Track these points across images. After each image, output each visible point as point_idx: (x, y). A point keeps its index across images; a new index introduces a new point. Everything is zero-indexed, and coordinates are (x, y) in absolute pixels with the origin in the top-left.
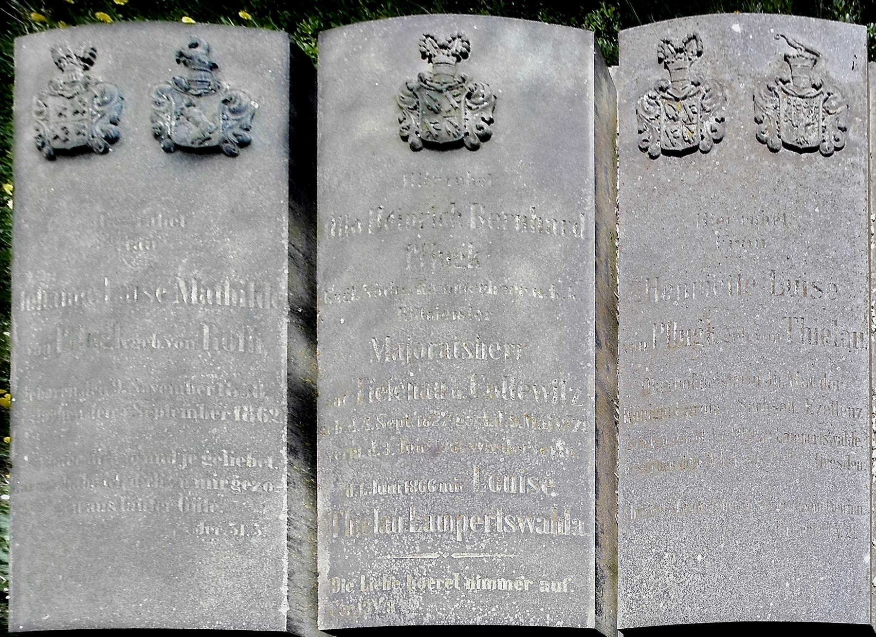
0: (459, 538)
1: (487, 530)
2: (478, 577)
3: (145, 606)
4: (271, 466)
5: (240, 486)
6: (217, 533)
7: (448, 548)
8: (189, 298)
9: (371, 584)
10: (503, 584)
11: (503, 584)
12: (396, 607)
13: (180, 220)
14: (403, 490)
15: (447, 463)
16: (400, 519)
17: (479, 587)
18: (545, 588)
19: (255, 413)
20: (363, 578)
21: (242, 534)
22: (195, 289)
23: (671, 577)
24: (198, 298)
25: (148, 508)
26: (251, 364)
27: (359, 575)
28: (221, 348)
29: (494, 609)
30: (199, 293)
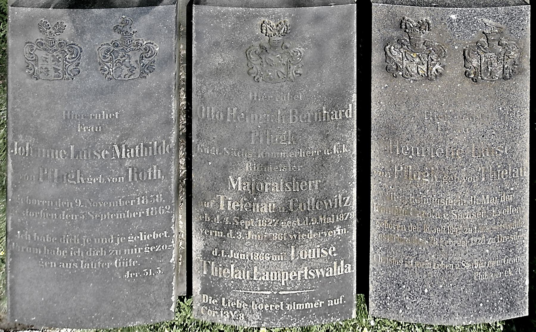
0: (283, 284)
1: (299, 279)
2: (294, 303)
3: (96, 318)
4: (166, 236)
5: (149, 250)
6: (137, 276)
7: (276, 289)
8: (121, 156)
9: (229, 303)
10: (308, 305)
11: (308, 305)
12: (245, 317)
13: (115, 115)
14: (250, 258)
15: (276, 245)
16: (248, 272)
17: (294, 308)
18: (331, 303)
19: (157, 210)
20: (224, 299)
21: (150, 274)
22: (124, 150)
23: (407, 298)
24: (126, 155)
25: (97, 266)
26: (155, 185)
27: (221, 297)
28: (138, 178)
29: (303, 319)
30: (126, 152)
